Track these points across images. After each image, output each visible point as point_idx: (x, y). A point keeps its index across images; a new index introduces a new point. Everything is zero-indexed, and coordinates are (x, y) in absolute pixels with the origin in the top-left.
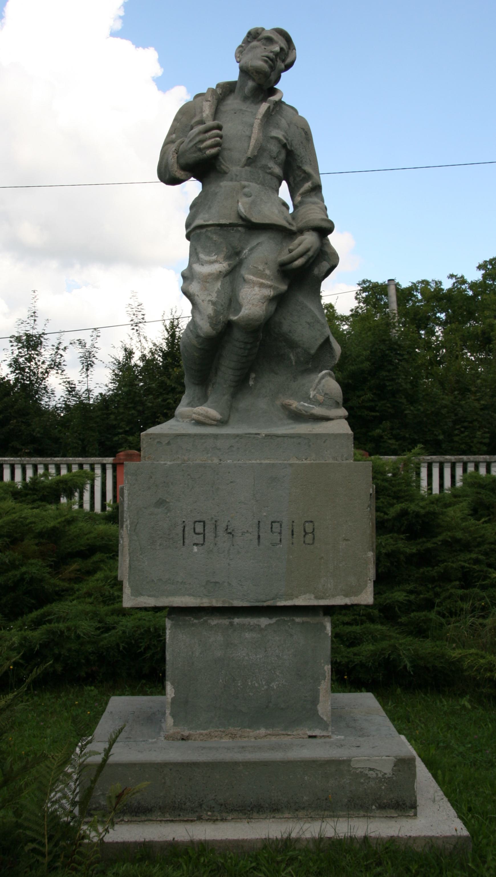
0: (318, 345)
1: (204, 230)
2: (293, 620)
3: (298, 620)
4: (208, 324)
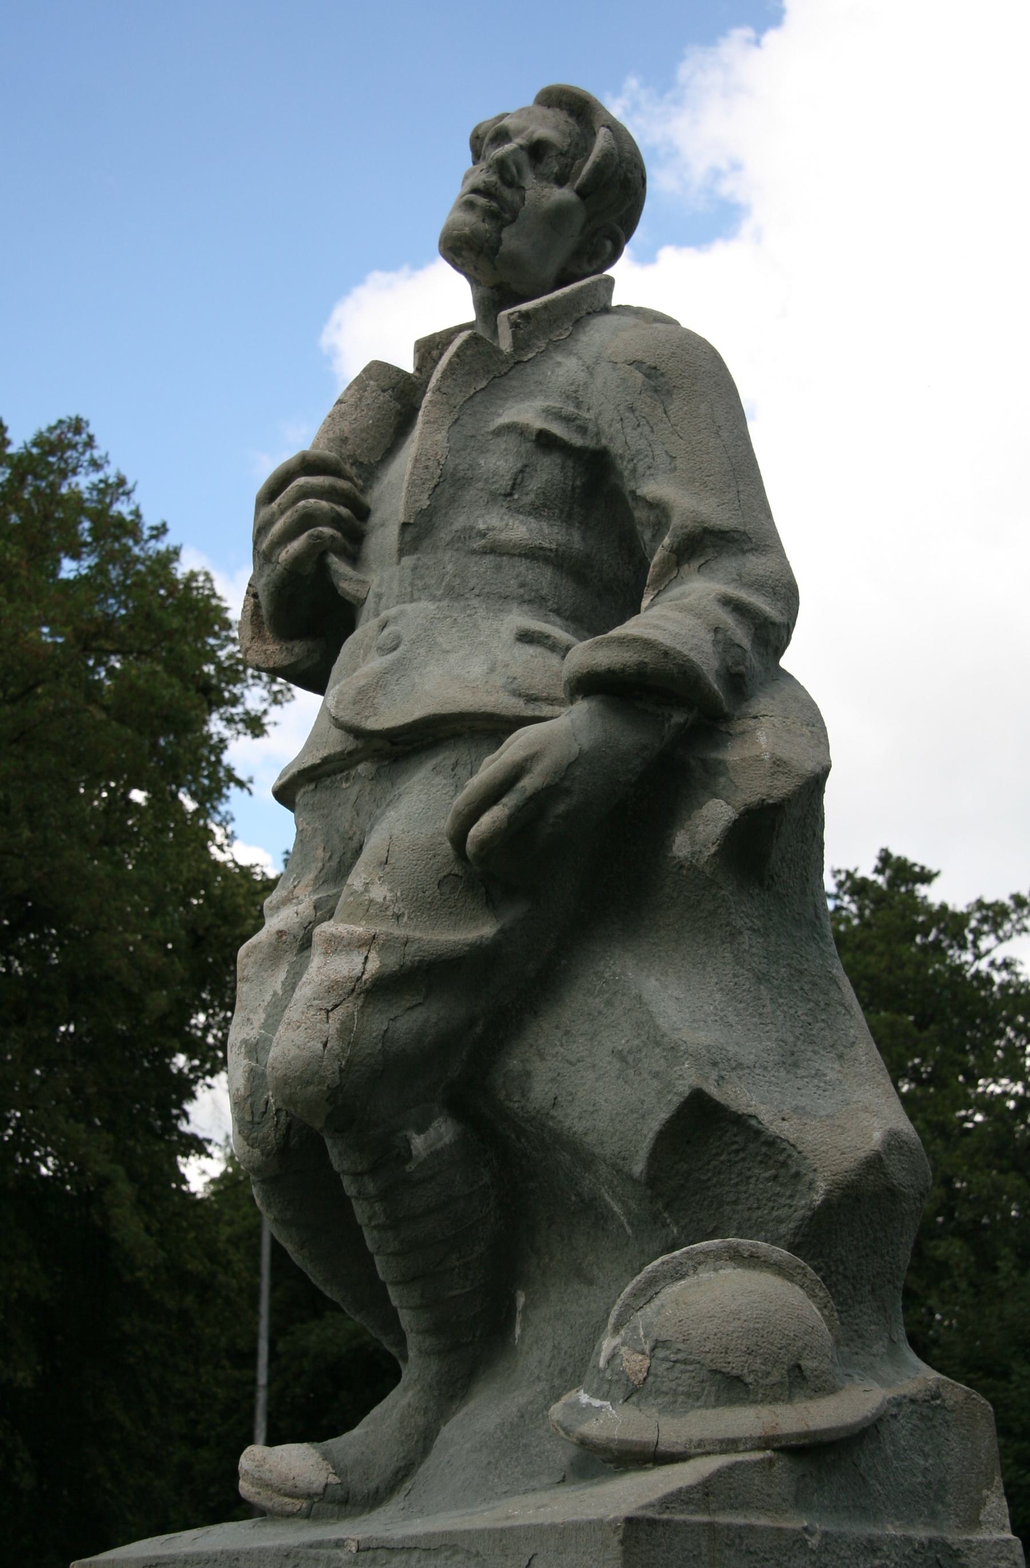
0: (651, 1135)
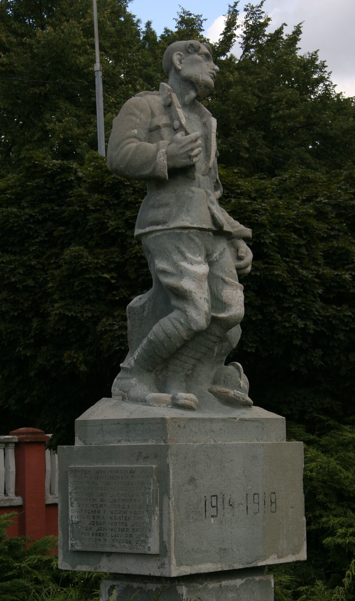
1: (187, 231)
2: (254, 579)
3: (257, 579)
4: (205, 320)
